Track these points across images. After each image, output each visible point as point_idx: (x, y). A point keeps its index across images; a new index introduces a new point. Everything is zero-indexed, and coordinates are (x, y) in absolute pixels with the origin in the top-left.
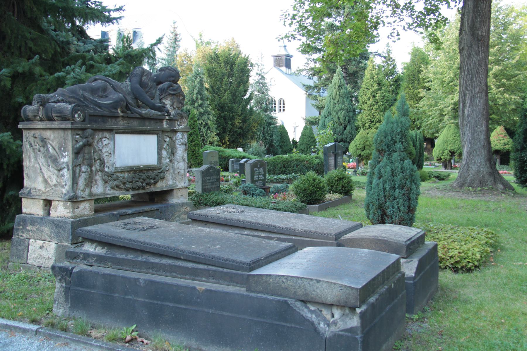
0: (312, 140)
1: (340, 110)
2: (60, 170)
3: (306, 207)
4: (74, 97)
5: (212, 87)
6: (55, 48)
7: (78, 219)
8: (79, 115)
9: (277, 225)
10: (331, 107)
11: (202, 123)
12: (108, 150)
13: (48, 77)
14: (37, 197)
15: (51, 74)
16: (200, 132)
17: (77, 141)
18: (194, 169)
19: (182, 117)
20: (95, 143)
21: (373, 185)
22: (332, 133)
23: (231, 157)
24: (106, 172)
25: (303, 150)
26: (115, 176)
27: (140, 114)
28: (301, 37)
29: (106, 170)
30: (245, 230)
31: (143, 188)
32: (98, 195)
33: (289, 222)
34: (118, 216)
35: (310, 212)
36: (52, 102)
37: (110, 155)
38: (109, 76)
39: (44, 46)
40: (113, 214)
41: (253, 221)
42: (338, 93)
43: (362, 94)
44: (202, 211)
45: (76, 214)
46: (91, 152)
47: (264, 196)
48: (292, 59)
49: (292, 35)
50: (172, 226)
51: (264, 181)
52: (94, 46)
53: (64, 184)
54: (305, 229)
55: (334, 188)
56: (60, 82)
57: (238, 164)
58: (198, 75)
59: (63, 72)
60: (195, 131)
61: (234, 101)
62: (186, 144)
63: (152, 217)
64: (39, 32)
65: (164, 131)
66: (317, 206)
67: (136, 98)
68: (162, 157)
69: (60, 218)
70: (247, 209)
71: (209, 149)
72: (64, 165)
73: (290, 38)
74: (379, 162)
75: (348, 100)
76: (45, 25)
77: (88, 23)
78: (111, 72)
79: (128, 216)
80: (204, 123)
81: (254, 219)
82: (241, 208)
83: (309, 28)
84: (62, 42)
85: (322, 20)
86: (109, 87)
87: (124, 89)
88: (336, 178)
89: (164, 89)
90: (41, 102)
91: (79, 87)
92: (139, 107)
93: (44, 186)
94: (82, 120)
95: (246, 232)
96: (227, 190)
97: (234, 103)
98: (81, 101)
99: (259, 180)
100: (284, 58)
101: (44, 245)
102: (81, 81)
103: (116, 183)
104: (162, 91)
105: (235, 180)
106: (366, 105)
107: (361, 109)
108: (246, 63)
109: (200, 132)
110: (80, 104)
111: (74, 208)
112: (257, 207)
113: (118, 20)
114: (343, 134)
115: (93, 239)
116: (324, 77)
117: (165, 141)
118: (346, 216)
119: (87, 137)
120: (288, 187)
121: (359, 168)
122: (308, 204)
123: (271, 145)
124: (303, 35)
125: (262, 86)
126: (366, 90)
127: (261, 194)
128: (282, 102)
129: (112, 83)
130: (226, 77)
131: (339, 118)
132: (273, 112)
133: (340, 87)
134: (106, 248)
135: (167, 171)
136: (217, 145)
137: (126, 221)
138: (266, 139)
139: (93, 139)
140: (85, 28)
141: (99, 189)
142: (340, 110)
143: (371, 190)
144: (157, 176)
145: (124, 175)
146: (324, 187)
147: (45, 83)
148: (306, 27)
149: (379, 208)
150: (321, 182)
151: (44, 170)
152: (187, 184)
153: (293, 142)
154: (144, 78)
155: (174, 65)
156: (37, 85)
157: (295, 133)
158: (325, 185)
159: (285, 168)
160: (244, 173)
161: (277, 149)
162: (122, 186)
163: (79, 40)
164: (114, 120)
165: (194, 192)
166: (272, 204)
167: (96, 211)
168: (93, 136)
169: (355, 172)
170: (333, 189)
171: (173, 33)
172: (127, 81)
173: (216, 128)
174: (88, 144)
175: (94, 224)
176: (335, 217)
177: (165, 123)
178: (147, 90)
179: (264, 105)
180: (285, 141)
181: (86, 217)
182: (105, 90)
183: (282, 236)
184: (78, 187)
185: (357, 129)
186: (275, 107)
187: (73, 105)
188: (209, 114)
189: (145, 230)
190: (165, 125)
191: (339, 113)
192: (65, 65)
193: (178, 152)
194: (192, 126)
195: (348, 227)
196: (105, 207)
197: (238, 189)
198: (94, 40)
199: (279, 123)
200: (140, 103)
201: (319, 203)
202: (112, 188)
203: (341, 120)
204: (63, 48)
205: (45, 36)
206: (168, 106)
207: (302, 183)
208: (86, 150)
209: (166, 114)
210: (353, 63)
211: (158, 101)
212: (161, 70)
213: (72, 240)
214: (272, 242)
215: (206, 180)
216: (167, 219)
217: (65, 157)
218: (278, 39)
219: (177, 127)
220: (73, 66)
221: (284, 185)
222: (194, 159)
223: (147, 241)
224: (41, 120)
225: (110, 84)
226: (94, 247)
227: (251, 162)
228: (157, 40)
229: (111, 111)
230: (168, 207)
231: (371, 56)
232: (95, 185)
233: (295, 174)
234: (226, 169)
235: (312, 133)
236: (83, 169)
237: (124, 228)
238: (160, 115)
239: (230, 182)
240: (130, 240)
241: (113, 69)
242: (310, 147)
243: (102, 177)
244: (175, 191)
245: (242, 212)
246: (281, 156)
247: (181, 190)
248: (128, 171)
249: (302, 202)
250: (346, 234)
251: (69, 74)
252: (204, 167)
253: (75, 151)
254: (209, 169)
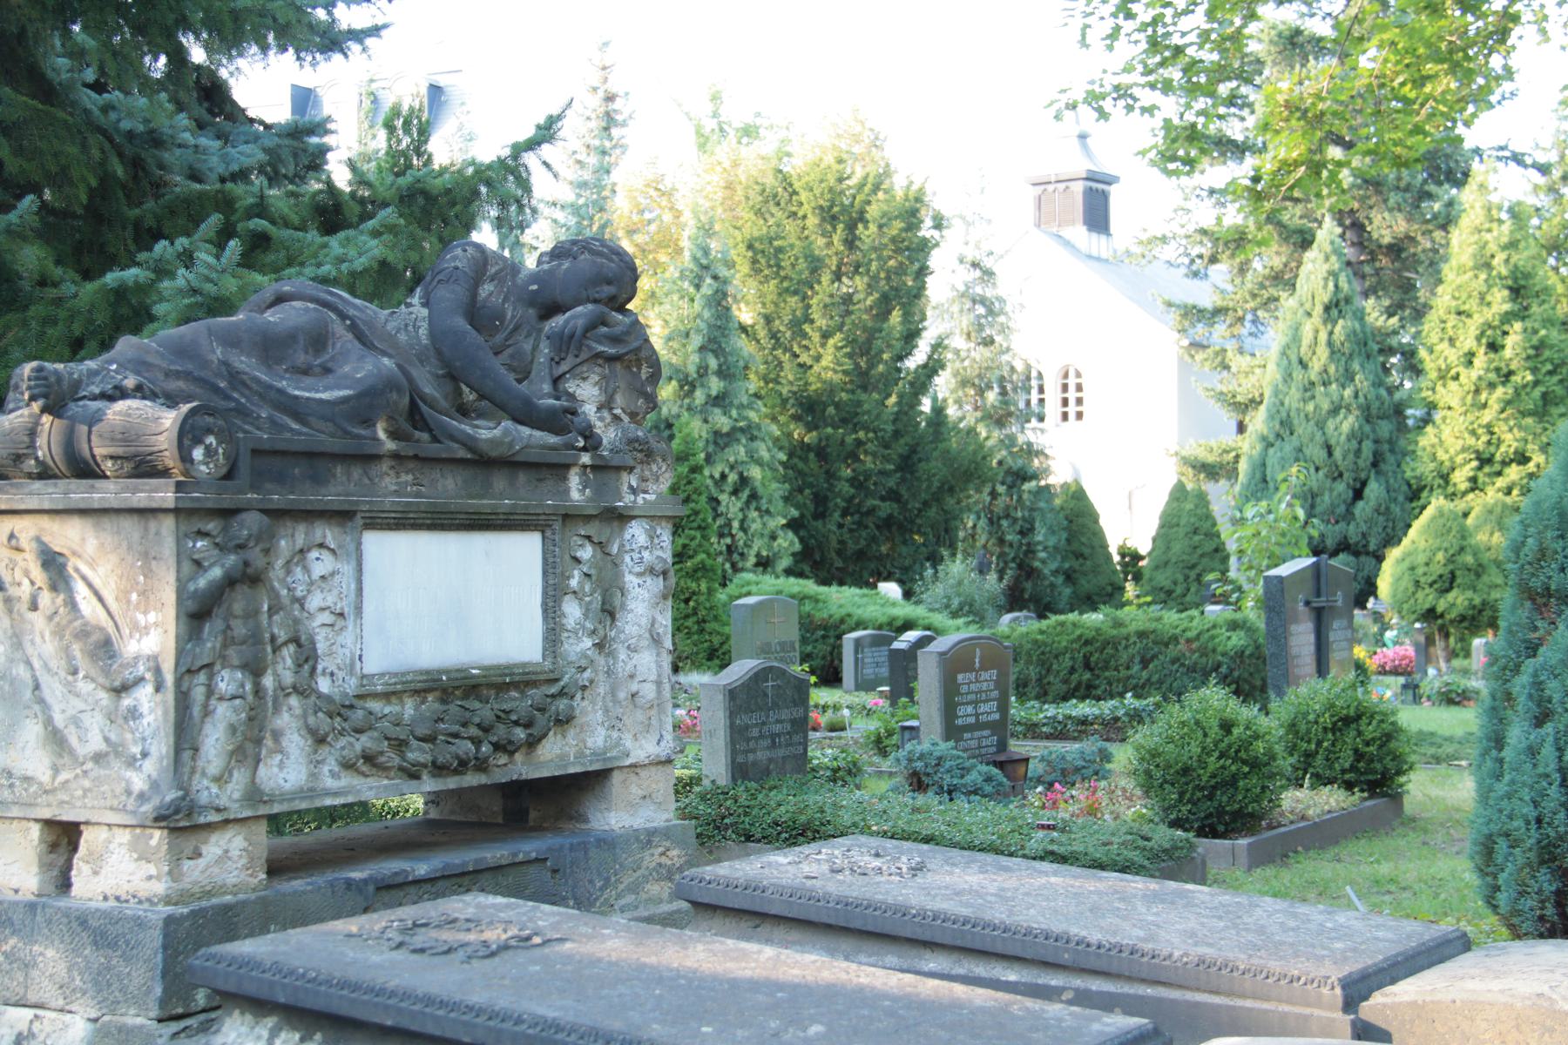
0: (1209, 546)
1: (1335, 411)
2: (121, 690)
3: (1192, 847)
4: (187, 376)
5: (768, 320)
6: (103, 163)
7: (195, 906)
8: (210, 453)
9: (1074, 930)
10: (1293, 398)
11: (724, 476)
13: (73, 289)
14: (15, 812)
15: (87, 275)
16: (717, 516)
17: (198, 563)
18: (695, 678)
19: (649, 455)
21: (1507, 754)
22: (1301, 513)
23: (852, 622)
24: (320, 696)
25: (1169, 593)
26: (360, 713)
27: (469, 443)
28: (1154, 97)
29: (324, 685)
30: (928, 954)
31: (482, 766)
32: (284, 797)
33: (1125, 918)
34: (371, 888)
35: (1212, 871)
36: (94, 398)
37: (340, 623)
38: (335, 282)
39: (55, 155)
40: (349, 883)
41: (965, 912)
42: (1323, 336)
43: (1434, 338)
44: (737, 864)
45: (186, 883)
46: (257, 612)
47: (1000, 795)
48: (1114, 191)
49: (1117, 88)
50: (610, 943)
51: (1001, 728)
52: (266, 150)
53: (136, 750)
54: (1203, 950)
55: (1319, 760)
56: (124, 311)
57: (882, 654)
58: (706, 268)
59: (138, 264)
60: (696, 513)
61: (862, 380)
62: (665, 573)
63: (517, 892)
64: (34, 97)
65: (570, 517)
66: (1243, 842)
67: (453, 377)
68: (563, 628)
69: (112, 903)
70: (935, 856)
71: (755, 591)
72: (141, 669)
73: (1107, 104)
74: (1532, 649)
75: (1370, 366)
76: (59, 65)
77: (241, 55)
78: (344, 267)
79: (412, 890)
80: (732, 477)
81: (967, 905)
82: (910, 853)
83: (1191, 51)
84: (130, 135)
85: (1252, 16)
86: (338, 328)
87: (402, 337)
88: (1327, 719)
89: (572, 336)
90: (46, 396)
91: (210, 332)
92: (464, 411)
93: (47, 762)
94: (224, 471)
95: (934, 962)
96: (836, 770)
97: (864, 388)
98: (216, 390)
100: (1078, 187)
101: (36, 1027)
102: (219, 306)
103: (365, 742)
104: (565, 343)
105: (873, 725)
106: (1453, 385)
107: (1432, 406)
108: (914, 213)
109: (717, 516)
110: (213, 406)
111: (176, 858)
112: (970, 847)
113: (369, 41)
114: (1348, 516)
115: (264, 993)
116: (1257, 264)
117: (577, 560)
118: (1380, 892)
119: (241, 547)
120: (1106, 757)
121: (1431, 671)
122: (1201, 833)
123: (1027, 571)
124: (1167, 87)
125: (986, 312)
126: (1452, 320)
127: (988, 789)
128: (1072, 381)
129: (352, 312)
130: (826, 278)
131: (1329, 450)
132: (1034, 422)
133: (1335, 308)
134: (318, 1036)
135: (584, 688)
136: (789, 572)
137: (408, 913)
138: (1001, 541)
139: (267, 551)
140: (223, 73)
141: (289, 770)
142: (1335, 411)
143: (1498, 777)
144: (542, 710)
145: (397, 708)
146: (1273, 758)
147: (62, 314)
148: (1178, 50)
149: (1542, 862)
150: (1256, 737)
151: (53, 690)
152: (668, 745)
153: (1123, 556)
154: (486, 289)
155: (603, 227)
156: (25, 324)
157: (1130, 523)
158: (1279, 749)
159: (1092, 670)
160: (910, 693)
161: (1052, 585)
162: (391, 758)
163: (201, 126)
164: (357, 472)
165: (694, 781)
166: (1041, 834)
167: (277, 868)
168: (266, 541)
169: (1412, 691)
170: (1312, 766)
171: (595, 89)
172: (415, 300)
173: (786, 499)
174: (248, 578)
175: (264, 930)
176: (1327, 893)
177: (574, 480)
178: (499, 338)
179: (992, 396)
180: (1086, 551)
181: (228, 898)
182: (319, 340)
183: (1096, 985)
184: (200, 763)
185: (1415, 494)
186: (1042, 401)
187: (185, 408)
188: (753, 439)
189: (493, 954)
190: (576, 491)
191: (1331, 424)
192: (148, 236)
193: (631, 605)
194: (683, 490)
195: (1399, 948)
196: (317, 855)
197: (886, 765)
198: (267, 127)
199: (1058, 476)
200: (469, 396)
201: (1251, 831)
202: (348, 766)
203: (1338, 454)
204: (136, 165)
205: (61, 114)
206: (589, 410)
207: (1170, 740)
208: (238, 602)
209: (581, 444)
210: (1393, 198)
211: (547, 387)
212: (558, 253)
213: (163, 1002)
214: (1055, 1009)
215: (747, 727)
216: (584, 903)
217: (145, 630)
218: (1052, 111)
219: (628, 498)
220: (182, 242)
221: (1090, 746)
222: (699, 639)
223: (503, 1002)
224: (45, 474)
225: (343, 316)
226: (265, 1034)
227: (942, 644)
228: (539, 127)
229: (346, 432)
230: (584, 846)
231: (1476, 165)
233: (1137, 696)
234: (831, 677)
235: (1208, 516)
236: (222, 686)
237: (400, 945)
238: (553, 448)
239: (848, 734)
240: (429, 1000)
241: (352, 253)
242: (1199, 578)
243: (305, 716)
244: (617, 778)
245: (917, 869)
246: (1072, 617)
247: (643, 773)
248: (416, 692)
249: (1176, 824)
250: (1393, 981)
251: (171, 275)
252: (740, 669)
253: (191, 605)
254: (759, 677)
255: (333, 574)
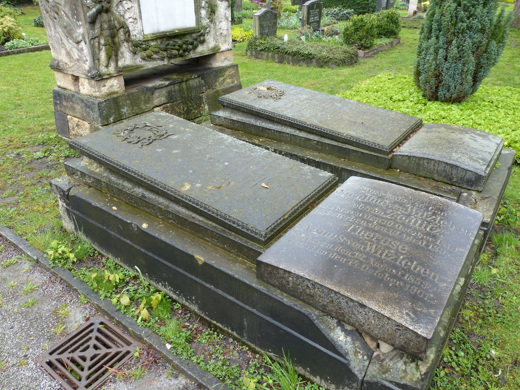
2: (78, 43)
12: (132, 15)
20: (114, 9)
29: (133, 38)
37: (136, 21)
99: (314, 22)
135: (207, 33)
232: (121, 58)
244: (218, 55)
253: (89, 20)
255: (131, 7)
